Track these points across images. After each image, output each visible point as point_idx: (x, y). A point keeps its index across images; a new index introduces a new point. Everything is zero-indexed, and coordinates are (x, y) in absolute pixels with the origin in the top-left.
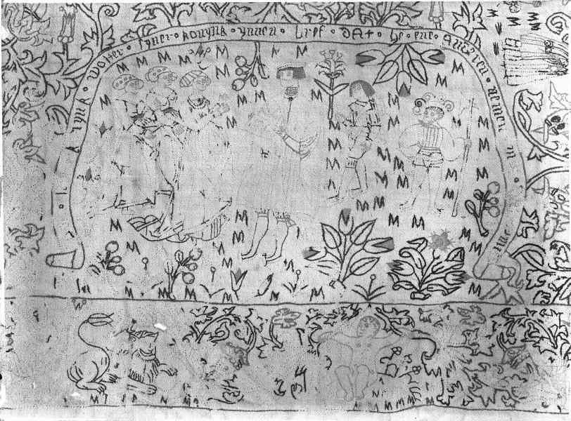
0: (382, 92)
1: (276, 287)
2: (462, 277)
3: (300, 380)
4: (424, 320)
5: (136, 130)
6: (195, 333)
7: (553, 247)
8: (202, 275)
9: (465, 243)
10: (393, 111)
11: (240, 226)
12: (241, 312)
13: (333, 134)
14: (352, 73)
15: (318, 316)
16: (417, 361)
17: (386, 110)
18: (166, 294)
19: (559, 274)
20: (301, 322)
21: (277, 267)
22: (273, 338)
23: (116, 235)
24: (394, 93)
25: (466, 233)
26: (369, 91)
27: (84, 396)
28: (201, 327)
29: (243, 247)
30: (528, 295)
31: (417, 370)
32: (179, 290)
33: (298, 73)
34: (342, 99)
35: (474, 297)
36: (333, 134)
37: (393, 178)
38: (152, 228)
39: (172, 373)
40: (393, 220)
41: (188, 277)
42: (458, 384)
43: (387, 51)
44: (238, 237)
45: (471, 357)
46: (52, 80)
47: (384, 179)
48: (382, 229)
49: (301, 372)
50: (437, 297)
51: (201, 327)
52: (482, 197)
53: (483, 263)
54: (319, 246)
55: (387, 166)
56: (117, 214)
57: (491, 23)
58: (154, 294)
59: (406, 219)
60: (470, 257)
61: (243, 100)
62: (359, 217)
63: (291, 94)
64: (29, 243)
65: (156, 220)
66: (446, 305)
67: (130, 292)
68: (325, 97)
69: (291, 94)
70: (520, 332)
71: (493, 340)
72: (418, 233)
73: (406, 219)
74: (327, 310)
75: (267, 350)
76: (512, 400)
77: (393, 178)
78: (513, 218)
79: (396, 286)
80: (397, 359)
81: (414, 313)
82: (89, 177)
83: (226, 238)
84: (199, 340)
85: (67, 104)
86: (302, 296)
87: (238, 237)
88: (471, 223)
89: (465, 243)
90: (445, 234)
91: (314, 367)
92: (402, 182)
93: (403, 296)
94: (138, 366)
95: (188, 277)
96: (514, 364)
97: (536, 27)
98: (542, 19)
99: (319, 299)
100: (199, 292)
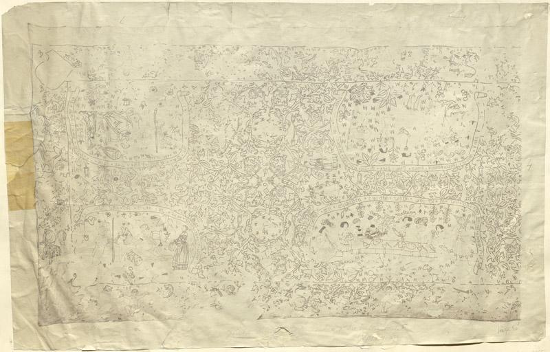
0: (377, 149)
1: (411, 86)
2: (350, 91)
3: (403, 57)
4: (362, 76)
5: (457, 137)
6: (437, 71)
7: (321, 102)
8: (435, 90)
9: (349, 101)
10: (373, 143)
11: (423, 105)
12: (422, 78)
13: (393, 135)
14: (386, 156)
15: (397, 77)
16: (365, 63)
17: (376, 144)
18: (448, 84)
19: (318, 94)
20: (403, 75)
21: (411, 92)
22: (412, 70)
23: (464, 103)
24: (373, 150)
25: (350, 105)
26: (381, 150)
27: (474, 50)
28: (435, 72)
29: (422, 99)
30: (329, 86)
31: (366, 61)
32: (443, 84)
33: (404, 155)
34: (390, 146)
35: (347, 84)
36: (393, 135)
37: (373, 122)
38: (452, 105)
39: (445, 58)
40: (373, 108)
41: (440, 89)
42: (352, 56)
43: (375, 164)
44: (423, 102)
45: (190, 285)
46: (485, 154)
47: (376, 122)
48: (376, 105)
49: (403, 59)
50: (359, 84)
51: (435, 72)
52: (344, 117)
53: (344, 95)
54: (397, 99)
55: (375, 125)
56: (465, 110)
57: (342, 174)
58: (452, 84)
59: (369, 108)
60: (348, 97)
61: (422, 146)
62: (385, 109)
63: (406, 148)
64: (492, 101)
65: (451, 108)
66: (356, 82)
67: (459, 84)
68: (395, 147)
69: (406, 148)
70: (332, 74)
71: (340, 70)
72: (365, 105)
73: (369, 108)
74: (394, 79)
75: (414, 65)
76: (15, 10)
77: (373, 122)
78: (335, 110)
79: (372, 87)
80: (371, 63)
81: (366, 79)
82: (473, 122)
83: (428, 101)
84: (436, 68)
85: (480, 146)
86: (402, 83)
87: (423, 102)
88: (348, 108)
89: (349, 101)
90: (356, 105)
91: (398, 61)
92: (370, 121)
93: (369, 84)
94: (456, 60)
95: (440, 89)
96: (334, 63)
97: (327, 174)
98: (325, 177)
99: (397, 82)
100: (436, 83)
